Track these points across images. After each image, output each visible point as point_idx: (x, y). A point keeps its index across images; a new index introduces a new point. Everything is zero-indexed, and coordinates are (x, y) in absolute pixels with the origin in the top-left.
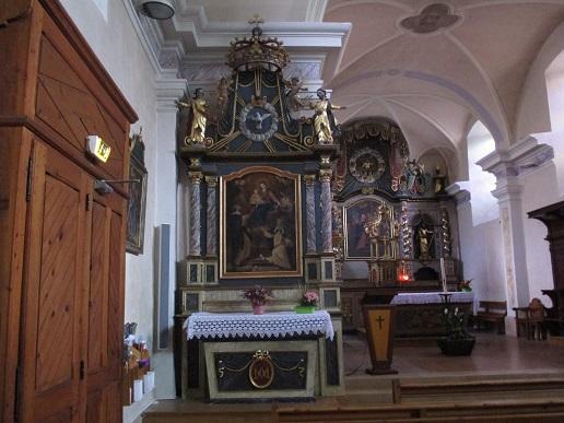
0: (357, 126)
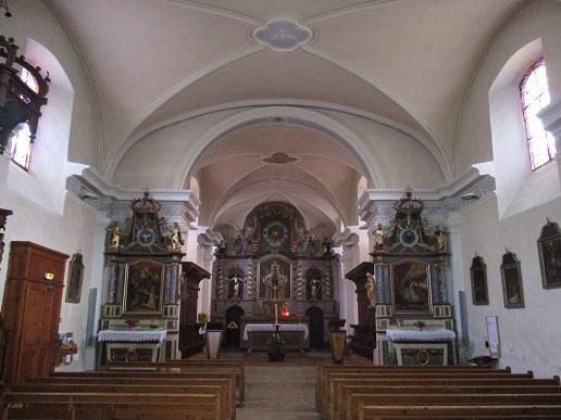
0: (266, 208)
